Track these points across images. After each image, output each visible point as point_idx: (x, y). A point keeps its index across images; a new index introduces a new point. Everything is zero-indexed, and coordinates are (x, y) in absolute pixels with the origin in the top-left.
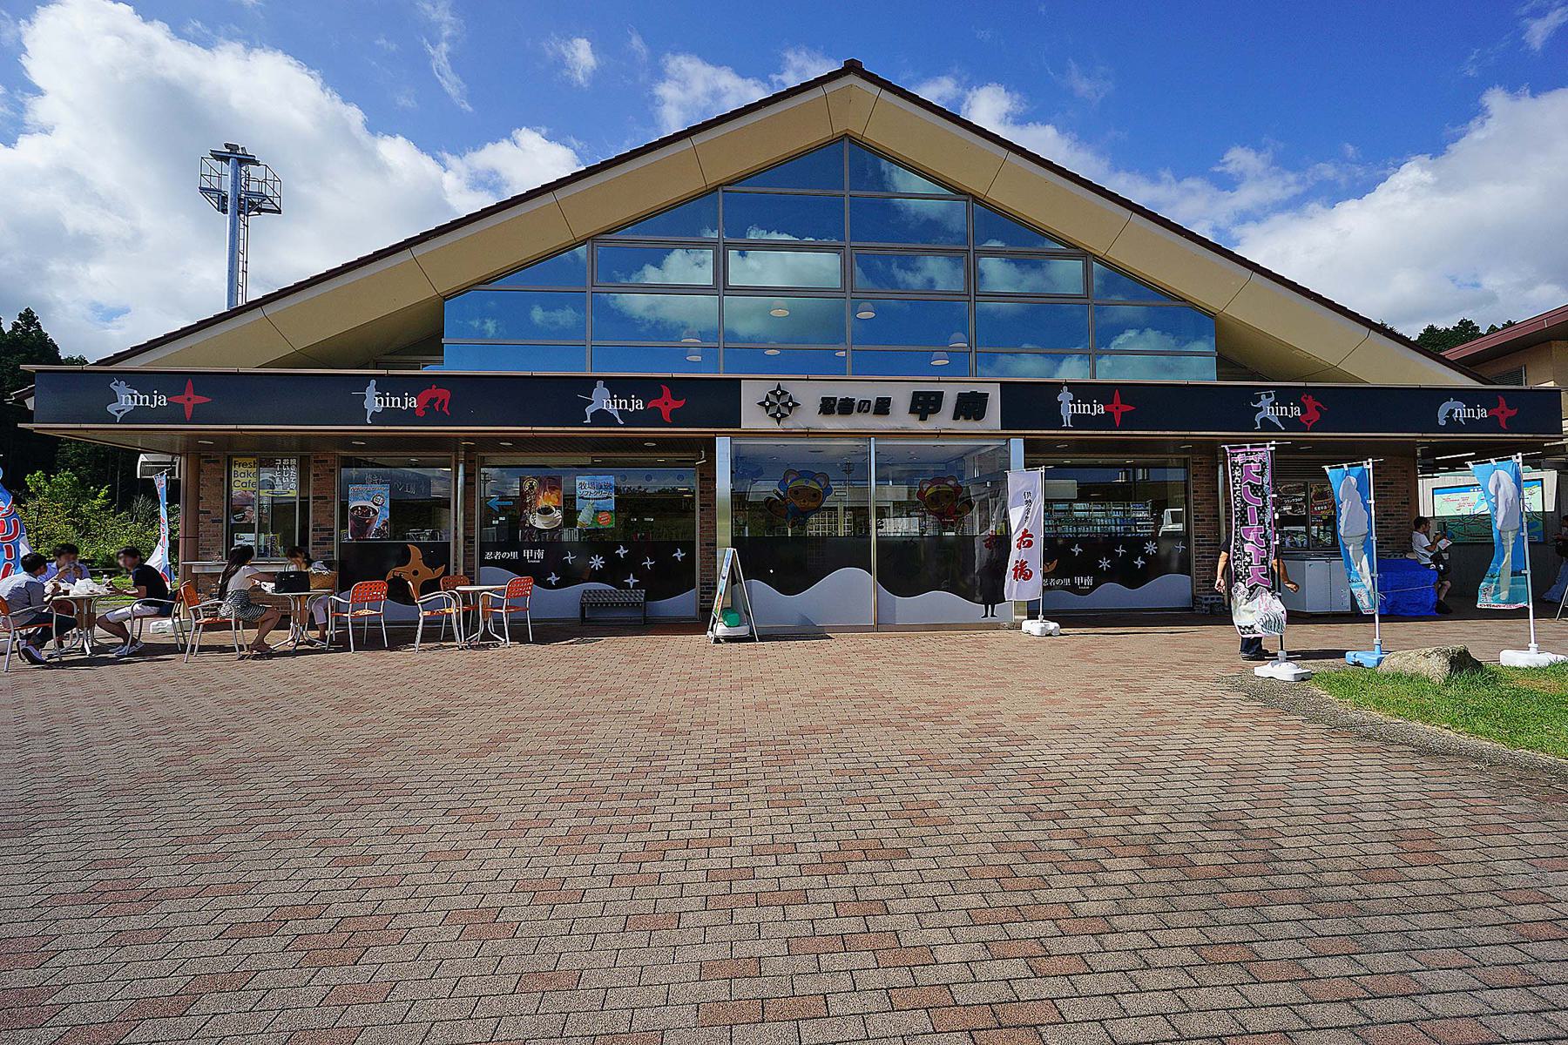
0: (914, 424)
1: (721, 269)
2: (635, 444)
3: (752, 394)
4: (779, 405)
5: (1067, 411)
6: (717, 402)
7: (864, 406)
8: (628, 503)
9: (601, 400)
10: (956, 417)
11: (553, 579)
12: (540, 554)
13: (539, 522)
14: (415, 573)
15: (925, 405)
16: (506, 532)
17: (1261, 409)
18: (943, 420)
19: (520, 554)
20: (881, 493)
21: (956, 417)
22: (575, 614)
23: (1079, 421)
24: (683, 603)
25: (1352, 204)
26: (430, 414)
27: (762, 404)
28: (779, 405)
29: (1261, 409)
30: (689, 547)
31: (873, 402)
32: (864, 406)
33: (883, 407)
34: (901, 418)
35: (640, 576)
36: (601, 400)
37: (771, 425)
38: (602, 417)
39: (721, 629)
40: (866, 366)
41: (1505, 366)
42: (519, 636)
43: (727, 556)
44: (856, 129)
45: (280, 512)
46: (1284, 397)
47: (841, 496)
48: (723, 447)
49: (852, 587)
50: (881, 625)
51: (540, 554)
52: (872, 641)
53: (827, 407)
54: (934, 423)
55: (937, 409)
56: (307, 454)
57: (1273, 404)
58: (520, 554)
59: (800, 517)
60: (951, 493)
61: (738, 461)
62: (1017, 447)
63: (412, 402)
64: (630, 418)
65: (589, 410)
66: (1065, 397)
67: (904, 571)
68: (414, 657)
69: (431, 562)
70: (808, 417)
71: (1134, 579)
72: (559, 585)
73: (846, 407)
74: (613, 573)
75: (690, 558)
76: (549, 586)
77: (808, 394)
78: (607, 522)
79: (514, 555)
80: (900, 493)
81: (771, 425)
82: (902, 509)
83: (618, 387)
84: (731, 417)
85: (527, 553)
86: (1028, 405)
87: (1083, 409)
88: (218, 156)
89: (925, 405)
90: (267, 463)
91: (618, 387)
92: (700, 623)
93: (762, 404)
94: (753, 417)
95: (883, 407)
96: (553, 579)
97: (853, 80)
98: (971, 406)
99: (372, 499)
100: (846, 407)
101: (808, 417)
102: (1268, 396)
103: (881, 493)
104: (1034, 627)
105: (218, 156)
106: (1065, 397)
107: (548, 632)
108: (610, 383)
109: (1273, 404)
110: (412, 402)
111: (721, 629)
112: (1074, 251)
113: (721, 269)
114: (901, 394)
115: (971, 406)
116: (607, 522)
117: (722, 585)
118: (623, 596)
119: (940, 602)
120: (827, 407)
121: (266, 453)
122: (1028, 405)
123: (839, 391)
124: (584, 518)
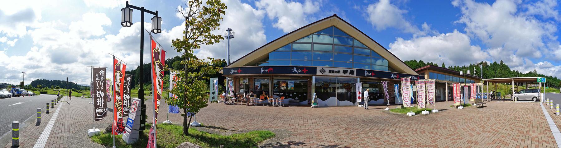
0: (343, 75)
1: (312, 47)
2: (299, 77)
3: (318, 69)
4: (323, 71)
5: (366, 74)
6: (313, 70)
7: (336, 72)
8: (296, 85)
9: (295, 70)
13: (282, 88)
15: (345, 72)
16: (277, 91)
18: (348, 74)
20: (337, 85)
22: (288, 103)
23: (368, 76)
24: (306, 102)
26: (270, 72)
28: (323, 71)
30: (307, 93)
32: (336, 72)
33: (339, 72)
34: (341, 74)
35: (298, 96)
36: (295, 70)
37: (321, 74)
38: (295, 73)
39: (313, 105)
40: (336, 65)
41: (422, 72)
42: (282, 106)
43: (314, 95)
44: (335, 25)
45: (246, 85)
46: (395, 74)
47: (331, 86)
48: (314, 77)
49: (333, 100)
50: (337, 106)
52: (336, 108)
53: (330, 72)
54: (346, 75)
56: (250, 78)
59: (325, 89)
60: (349, 85)
61: (316, 79)
62: (359, 79)
63: (267, 70)
64: (299, 73)
66: (366, 72)
67: (341, 97)
68: (268, 107)
69: (266, 94)
70: (327, 73)
71: (376, 99)
73: (333, 72)
74: (294, 97)
75: (307, 95)
77: (327, 70)
78: (293, 89)
80: (341, 85)
81: (321, 74)
82: (341, 88)
83: (298, 68)
84: (315, 73)
86: (360, 73)
87: (368, 74)
89: (345, 72)
90: (244, 79)
91: (298, 68)
92: (310, 105)
94: (318, 73)
95: (339, 72)
97: (335, 17)
98: (352, 72)
99: (258, 84)
100: (333, 72)
101: (327, 73)
103: (337, 85)
104: (360, 106)
106: (366, 72)
107: (286, 105)
108: (296, 67)
110: (267, 70)
111: (313, 105)
112: (369, 48)
113: (312, 47)
114: (341, 70)
115: (352, 72)
116: (293, 89)
117: (313, 99)
118: (295, 101)
119: (347, 102)
120: (330, 72)
121: (244, 78)
122: (360, 73)
123: (332, 69)
124: (289, 88)
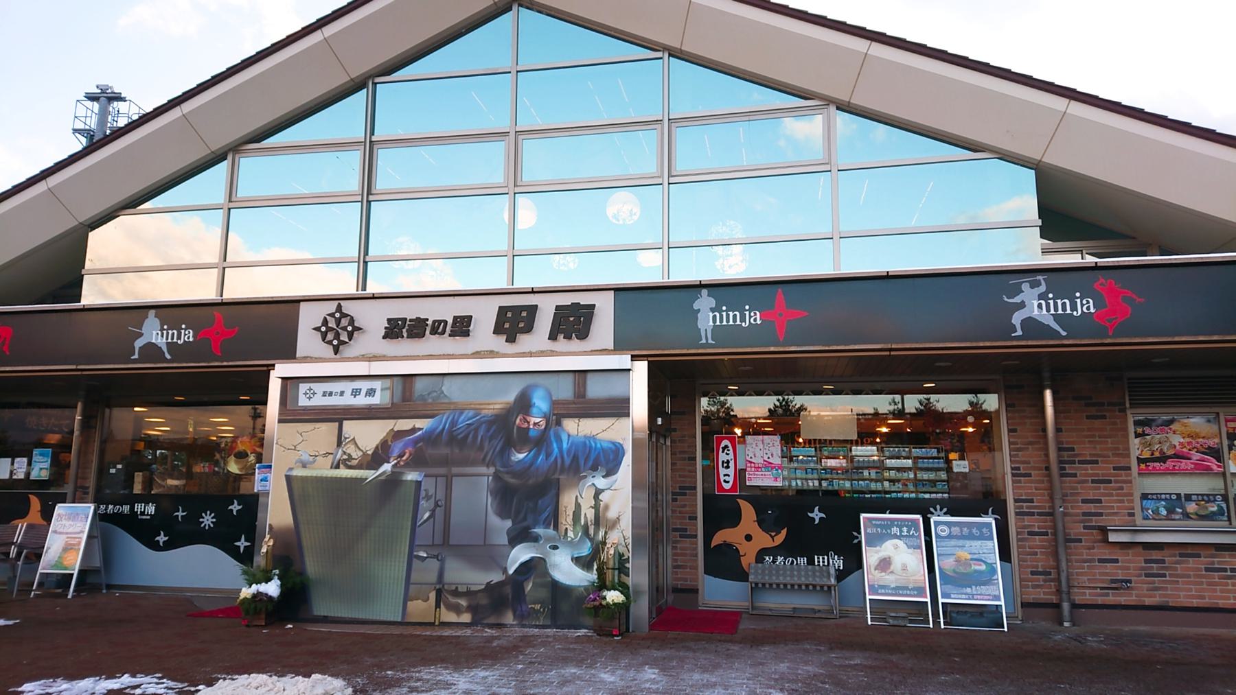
10: (553, 337)
11: (162, 538)
12: (151, 509)
14: (749, 538)
17: (1022, 305)
19: (132, 508)
21: (553, 337)
25: (810, 11)
27: (318, 329)
29: (1022, 305)
31: (450, 321)
32: (438, 328)
51: (151, 509)
55: (529, 329)
57: (1042, 296)
58: (132, 508)
65: (139, 343)
72: (168, 546)
76: (155, 547)
79: (126, 508)
85: (139, 508)
88: (92, 98)
93: (318, 329)
96: (162, 538)
102: (1035, 285)
105: (92, 98)
109: (1042, 296)
113: (668, 152)
